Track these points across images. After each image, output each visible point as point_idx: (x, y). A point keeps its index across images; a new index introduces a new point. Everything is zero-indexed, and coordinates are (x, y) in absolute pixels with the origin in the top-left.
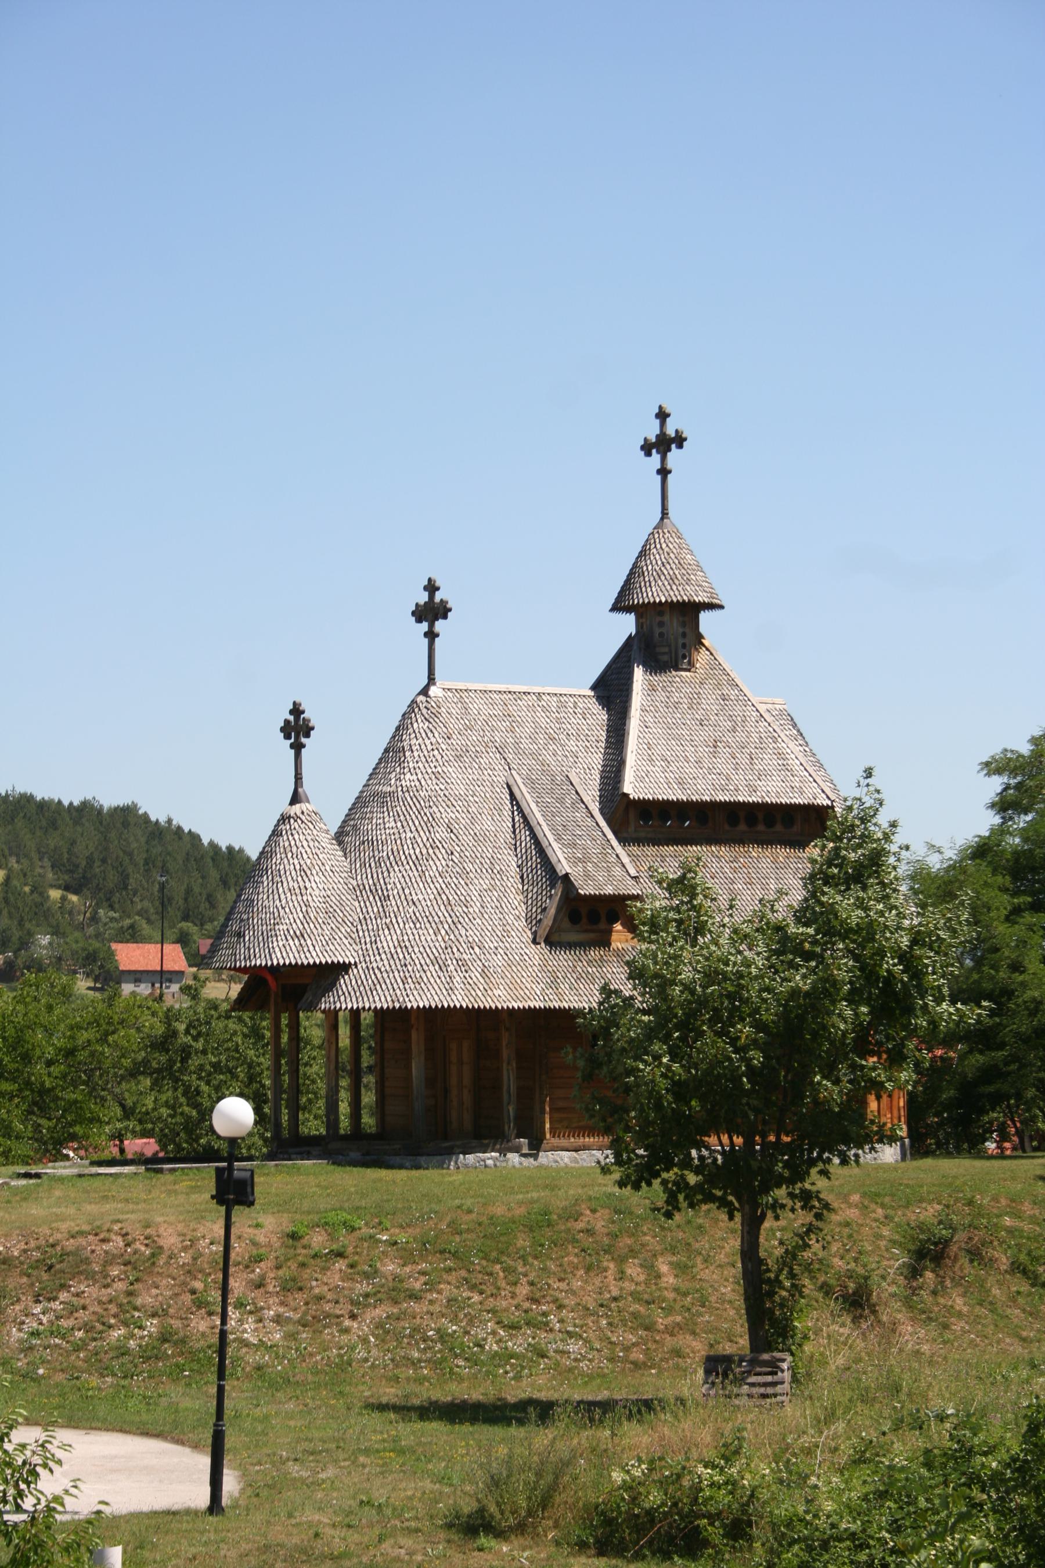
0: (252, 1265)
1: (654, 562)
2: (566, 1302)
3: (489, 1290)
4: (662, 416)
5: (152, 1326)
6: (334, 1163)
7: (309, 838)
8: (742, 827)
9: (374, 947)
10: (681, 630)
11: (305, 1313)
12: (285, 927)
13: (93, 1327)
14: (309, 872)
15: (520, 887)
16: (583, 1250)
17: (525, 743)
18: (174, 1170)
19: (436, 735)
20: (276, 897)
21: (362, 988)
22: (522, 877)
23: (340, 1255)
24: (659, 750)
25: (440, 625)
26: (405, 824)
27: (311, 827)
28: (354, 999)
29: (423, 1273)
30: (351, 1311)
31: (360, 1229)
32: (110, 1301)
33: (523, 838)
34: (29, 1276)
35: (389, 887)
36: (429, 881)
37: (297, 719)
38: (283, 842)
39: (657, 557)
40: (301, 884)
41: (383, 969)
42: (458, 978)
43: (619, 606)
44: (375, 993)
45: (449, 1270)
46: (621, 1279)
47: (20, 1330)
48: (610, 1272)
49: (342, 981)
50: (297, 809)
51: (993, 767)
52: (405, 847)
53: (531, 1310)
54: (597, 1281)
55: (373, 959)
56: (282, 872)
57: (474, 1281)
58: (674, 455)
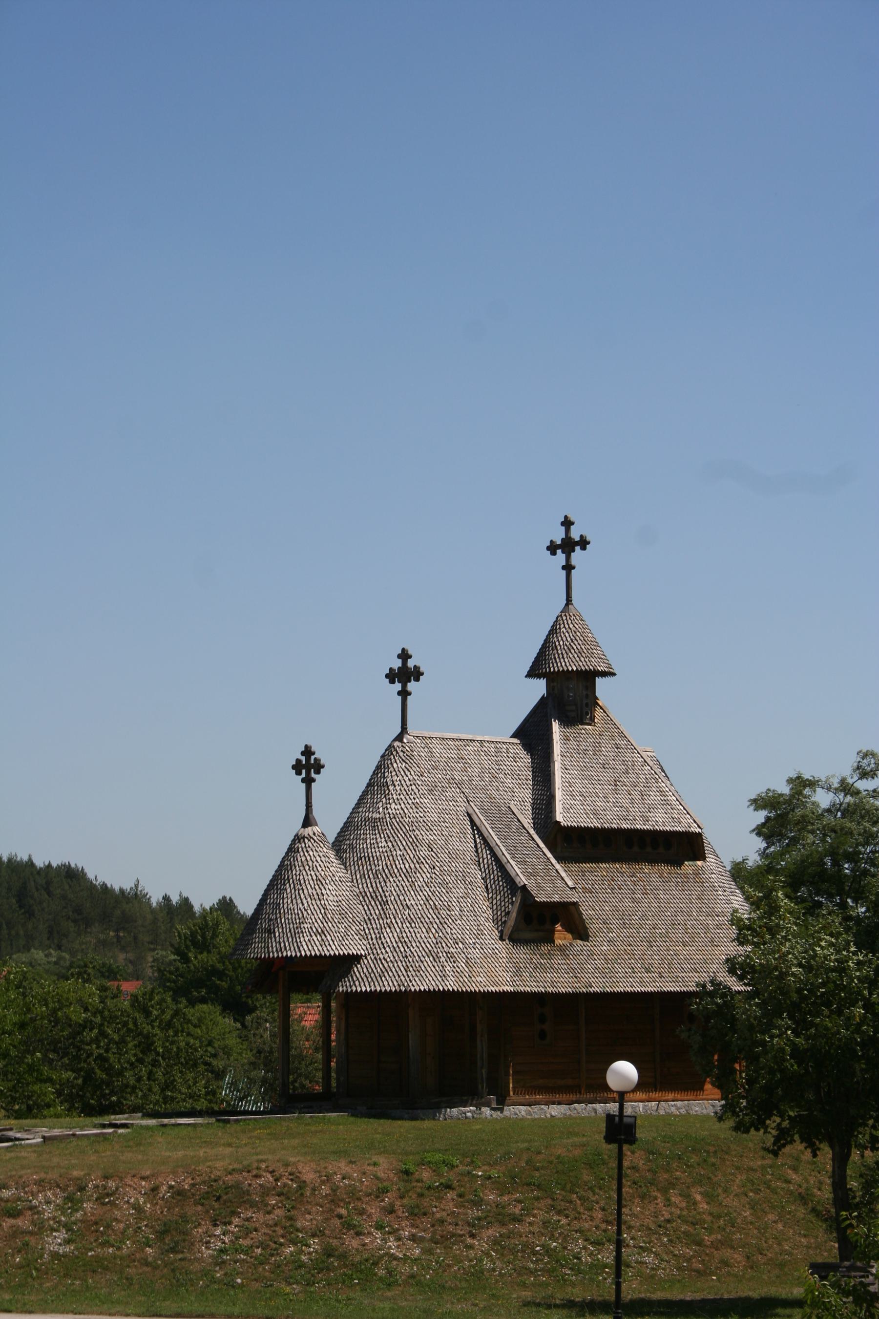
0: (381, 1195)
1: (564, 639)
2: (632, 1223)
3: (572, 1214)
4: (567, 523)
5: (315, 1244)
6: (352, 1115)
7: (321, 854)
8: (636, 849)
9: (380, 942)
10: (585, 693)
11: (434, 1233)
12: (309, 926)
13: (268, 1246)
14: (323, 882)
15: (486, 895)
16: (635, 1183)
17: (476, 781)
18: (237, 1121)
19: (413, 773)
20: (299, 901)
21: (372, 975)
22: (486, 887)
23: (449, 1187)
24: (578, 787)
25: (412, 686)
26: (395, 844)
27: (322, 845)
28: (367, 984)
29: (519, 1201)
30: (470, 1232)
31: (457, 1166)
32: (276, 1225)
33: (485, 856)
34: (202, 1205)
35: (387, 894)
36: (418, 889)
37: (308, 759)
38: (301, 857)
39: (567, 634)
40: (319, 891)
41: (388, 960)
42: (448, 968)
43: (534, 672)
44: (383, 978)
45: (537, 1199)
46: (669, 1205)
47: (208, 1248)
48: (659, 1200)
49: (355, 969)
50: (309, 831)
51: (758, 803)
52: (397, 862)
53: (608, 1229)
54: (652, 1207)
55: (379, 952)
56: (302, 882)
57: (559, 1208)
58: (577, 555)
